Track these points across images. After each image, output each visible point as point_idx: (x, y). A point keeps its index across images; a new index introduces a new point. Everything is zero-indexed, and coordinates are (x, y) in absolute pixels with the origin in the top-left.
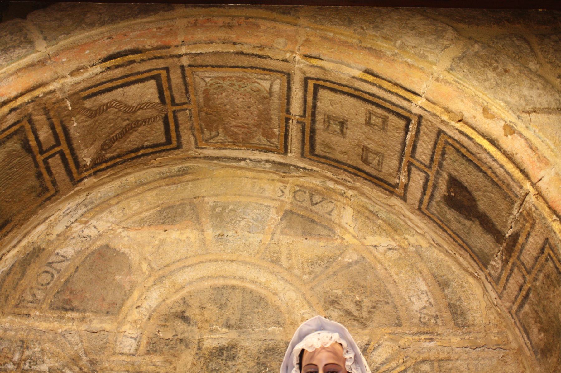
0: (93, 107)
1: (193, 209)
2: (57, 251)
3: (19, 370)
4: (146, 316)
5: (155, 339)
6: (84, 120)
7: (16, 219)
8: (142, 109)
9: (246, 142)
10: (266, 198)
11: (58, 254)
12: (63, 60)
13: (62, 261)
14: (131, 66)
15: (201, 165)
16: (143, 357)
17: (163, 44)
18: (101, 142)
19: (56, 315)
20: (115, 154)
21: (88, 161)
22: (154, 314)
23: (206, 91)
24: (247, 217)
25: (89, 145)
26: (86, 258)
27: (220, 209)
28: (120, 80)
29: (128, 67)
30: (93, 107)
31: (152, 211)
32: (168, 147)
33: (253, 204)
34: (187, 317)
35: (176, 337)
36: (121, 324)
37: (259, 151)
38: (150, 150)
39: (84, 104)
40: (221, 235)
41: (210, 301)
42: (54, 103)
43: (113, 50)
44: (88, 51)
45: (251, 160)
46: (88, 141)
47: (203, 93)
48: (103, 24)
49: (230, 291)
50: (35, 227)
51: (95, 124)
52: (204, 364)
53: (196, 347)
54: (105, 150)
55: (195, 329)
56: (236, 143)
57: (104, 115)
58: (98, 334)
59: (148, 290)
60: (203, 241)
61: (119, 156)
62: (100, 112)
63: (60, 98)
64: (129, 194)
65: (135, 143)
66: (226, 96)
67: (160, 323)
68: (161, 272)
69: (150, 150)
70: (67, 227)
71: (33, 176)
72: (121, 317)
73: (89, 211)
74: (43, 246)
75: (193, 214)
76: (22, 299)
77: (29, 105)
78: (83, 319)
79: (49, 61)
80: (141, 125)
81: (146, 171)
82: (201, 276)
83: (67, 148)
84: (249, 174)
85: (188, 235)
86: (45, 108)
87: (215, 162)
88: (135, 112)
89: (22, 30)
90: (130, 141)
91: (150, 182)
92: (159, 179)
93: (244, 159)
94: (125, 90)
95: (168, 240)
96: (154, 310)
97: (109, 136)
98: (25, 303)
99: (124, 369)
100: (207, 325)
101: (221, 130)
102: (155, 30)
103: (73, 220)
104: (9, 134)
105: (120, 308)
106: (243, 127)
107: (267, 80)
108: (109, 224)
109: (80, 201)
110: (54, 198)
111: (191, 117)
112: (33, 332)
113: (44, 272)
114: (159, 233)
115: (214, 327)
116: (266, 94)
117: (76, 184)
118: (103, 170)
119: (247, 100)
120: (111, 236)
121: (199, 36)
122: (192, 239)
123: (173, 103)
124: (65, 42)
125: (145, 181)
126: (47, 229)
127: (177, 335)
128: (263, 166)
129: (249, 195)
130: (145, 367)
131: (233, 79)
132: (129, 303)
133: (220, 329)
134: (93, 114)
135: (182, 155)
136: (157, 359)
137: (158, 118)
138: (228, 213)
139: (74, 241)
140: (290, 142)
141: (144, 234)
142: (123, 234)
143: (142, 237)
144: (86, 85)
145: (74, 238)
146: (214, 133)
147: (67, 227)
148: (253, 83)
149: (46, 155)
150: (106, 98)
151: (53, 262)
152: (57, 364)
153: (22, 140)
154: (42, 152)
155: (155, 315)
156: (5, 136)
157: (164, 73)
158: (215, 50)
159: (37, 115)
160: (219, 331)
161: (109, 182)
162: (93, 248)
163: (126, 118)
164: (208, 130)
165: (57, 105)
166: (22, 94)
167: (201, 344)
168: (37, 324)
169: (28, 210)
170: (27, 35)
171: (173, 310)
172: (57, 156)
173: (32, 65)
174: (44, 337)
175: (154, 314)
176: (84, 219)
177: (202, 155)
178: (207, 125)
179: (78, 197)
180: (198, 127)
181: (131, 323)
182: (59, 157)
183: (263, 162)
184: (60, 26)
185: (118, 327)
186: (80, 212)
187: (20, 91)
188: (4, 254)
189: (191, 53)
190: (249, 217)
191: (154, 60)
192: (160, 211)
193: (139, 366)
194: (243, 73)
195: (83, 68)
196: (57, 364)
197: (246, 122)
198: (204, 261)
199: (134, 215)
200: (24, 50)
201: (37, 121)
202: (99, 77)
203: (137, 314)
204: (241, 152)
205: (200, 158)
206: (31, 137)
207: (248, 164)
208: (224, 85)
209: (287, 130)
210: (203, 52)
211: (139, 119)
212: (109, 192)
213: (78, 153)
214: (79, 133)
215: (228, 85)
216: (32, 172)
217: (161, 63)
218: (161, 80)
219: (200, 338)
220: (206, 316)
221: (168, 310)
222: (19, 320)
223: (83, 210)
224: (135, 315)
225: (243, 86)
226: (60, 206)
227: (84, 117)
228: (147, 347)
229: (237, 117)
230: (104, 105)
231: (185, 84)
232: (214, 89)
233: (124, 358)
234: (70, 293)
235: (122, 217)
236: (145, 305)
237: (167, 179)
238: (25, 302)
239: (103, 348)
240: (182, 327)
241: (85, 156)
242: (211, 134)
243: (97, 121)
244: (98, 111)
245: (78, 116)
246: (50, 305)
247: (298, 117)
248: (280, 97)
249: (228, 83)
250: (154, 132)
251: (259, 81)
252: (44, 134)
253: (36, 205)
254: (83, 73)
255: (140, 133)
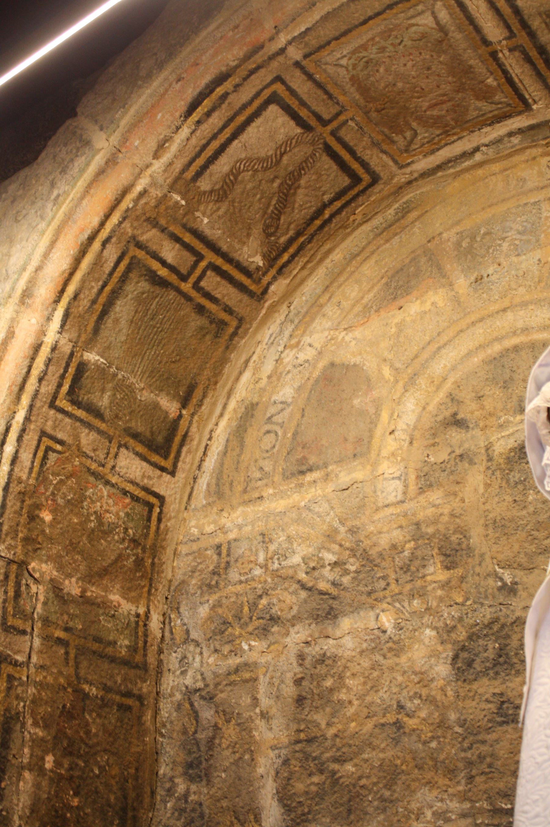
0: (215, 185)
1: (430, 259)
2: (272, 400)
3: (268, 572)
4: (404, 440)
5: (426, 469)
6: (215, 208)
7: (202, 380)
8: (285, 152)
9: (457, 123)
10: (531, 191)
11: (275, 403)
12: (136, 144)
13: (282, 410)
14: (227, 102)
15: (424, 190)
16: (415, 501)
17: (250, 48)
18: (260, 226)
19: (293, 485)
20: (291, 233)
21: (259, 261)
22: (416, 433)
23: (354, 80)
24: (510, 234)
25: (245, 239)
26: (311, 392)
27: (468, 240)
28: (226, 130)
29: (224, 106)
30: (215, 185)
31: (376, 289)
32: (361, 187)
33: (514, 210)
34: (462, 419)
35: (453, 455)
36: (375, 465)
37: (490, 125)
38: (338, 204)
39: (199, 187)
40: (479, 280)
41: (488, 383)
42: (156, 207)
43: (191, 93)
44: (160, 115)
45: (486, 146)
46: (239, 233)
47: (353, 85)
48: (160, 66)
49: (513, 356)
50: (237, 379)
51: (233, 206)
52: (502, 479)
53: (485, 458)
54: (272, 235)
55: (477, 432)
56: (448, 131)
57: (238, 189)
58: (350, 490)
59: (399, 404)
60: (456, 300)
61: (299, 234)
62: (228, 186)
63: (160, 195)
64: (342, 279)
65: (309, 205)
66: (386, 70)
67: (426, 443)
68: (409, 371)
69: (338, 204)
70: (277, 361)
71: (193, 314)
72: (373, 455)
73: (296, 327)
74: (255, 400)
75: (431, 266)
76: (248, 480)
77: (123, 225)
78: (327, 477)
79: (120, 155)
80: (300, 175)
81: (353, 236)
82: (466, 351)
83: (216, 257)
84: (495, 167)
85: (432, 300)
86: (148, 220)
87: (440, 174)
88: (278, 162)
89: (75, 132)
90: (301, 206)
91: (364, 249)
92: (374, 239)
93: (477, 149)
94: (243, 140)
95: (408, 319)
96: (415, 428)
97: (265, 213)
98: (252, 484)
99: (395, 526)
100: (492, 421)
101: (414, 125)
102: (231, 33)
103: (281, 348)
104: (120, 275)
105: (369, 442)
106: (443, 102)
107: (423, 12)
108: (326, 333)
109: (283, 318)
110: (240, 331)
111: (361, 128)
112: (272, 518)
113: (265, 434)
114: (393, 316)
115: (502, 420)
116: (438, 35)
117: (262, 299)
118: (289, 262)
119: (418, 59)
120: (333, 348)
121: (291, 6)
122: (441, 304)
123: (324, 123)
124: (125, 121)
125: (355, 250)
126: (254, 374)
127: (454, 452)
128: (509, 145)
129: (503, 200)
130: (422, 514)
131: (377, 39)
132: (378, 432)
133: (512, 419)
134: (222, 193)
135: (387, 190)
136: (435, 496)
137: (317, 154)
138: (482, 238)
139: (290, 376)
140: (522, 87)
141: (374, 327)
142: (347, 338)
143: (373, 331)
144: (184, 160)
145: (289, 372)
146: (408, 134)
147: (277, 361)
148: (407, 29)
149: (192, 279)
150: (225, 164)
151: (272, 416)
152: (310, 550)
153: (145, 275)
154: (184, 278)
155: (417, 434)
156: (116, 280)
157: (278, 87)
158: (323, 13)
159: (143, 234)
160: (512, 422)
161: (310, 275)
162: (316, 374)
163: (272, 177)
164: (397, 134)
165: (163, 207)
166: (107, 216)
167: (490, 452)
168: (273, 505)
169: (214, 360)
170: (81, 136)
171: (439, 418)
172: (209, 273)
173: (101, 173)
174: (286, 519)
175: (416, 433)
176: (294, 341)
177: (416, 175)
178: (391, 128)
179: (276, 315)
180: (380, 137)
181: (389, 458)
182: (213, 274)
183: (506, 139)
184: (114, 100)
185: (373, 471)
186: (287, 333)
187: (102, 214)
188: (212, 431)
189: (294, 39)
190: (513, 232)
191: (253, 77)
192: (387, 284)
193: (414, 515)
194: (385, 22)
195: (166, 141)
196: (310, 550)
197: (441, 92)
198: (464, 327)
199: (353, 306)
200: (83, 158)
201: (148, 241)
202: (194, 141)
203: (393, 443)
204: (465, 140)
205: (416, 179)
206: (155, 265)
207: (487, 154)
208: (372, 56)
209: (505, 72)
210: (308, 25)
211: (291, 168)
212: (315, 289)
213: (236, 256)
214: (219, 229)
215: (377, 53)
216: (187, 309)
217: (264, 77)
218: (283, 99)
219: (486, 443)
220: (487, 407)
221: (433, 420)
222: (252, 508)
223: (290, 328)
224: (391, 444)
225: (398, 41)
226: (259, 337)
227: (211, 205)
228: (417, 484)
229: (423, 93)
230: (228, 175)
231: (319, 85)
232: (362, 70)
233: (391, 510)
234: (303, 448)
235: (340, 314)
236: (401, 425)
237: (385, 234)
238: (253, 482)
239: (361, 507)
240: (458, 437)
241: (249, 256)
242: (405, 138)
243: (233, 201)
244: (225, 187)
245: (202, 208)
246: (283, 474)
247: (504, 42)
248: (459, 28)
249: (374, 50)
250: (325, 177)
251: (413, 21)
252: (170, 252)
253: (220, 350)
254: (169, 147)
255: (306, 188)
